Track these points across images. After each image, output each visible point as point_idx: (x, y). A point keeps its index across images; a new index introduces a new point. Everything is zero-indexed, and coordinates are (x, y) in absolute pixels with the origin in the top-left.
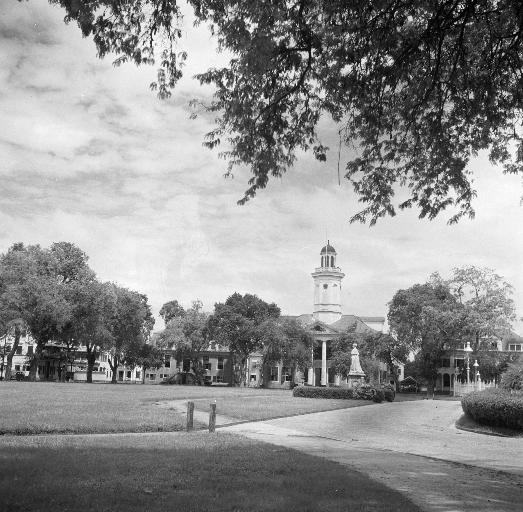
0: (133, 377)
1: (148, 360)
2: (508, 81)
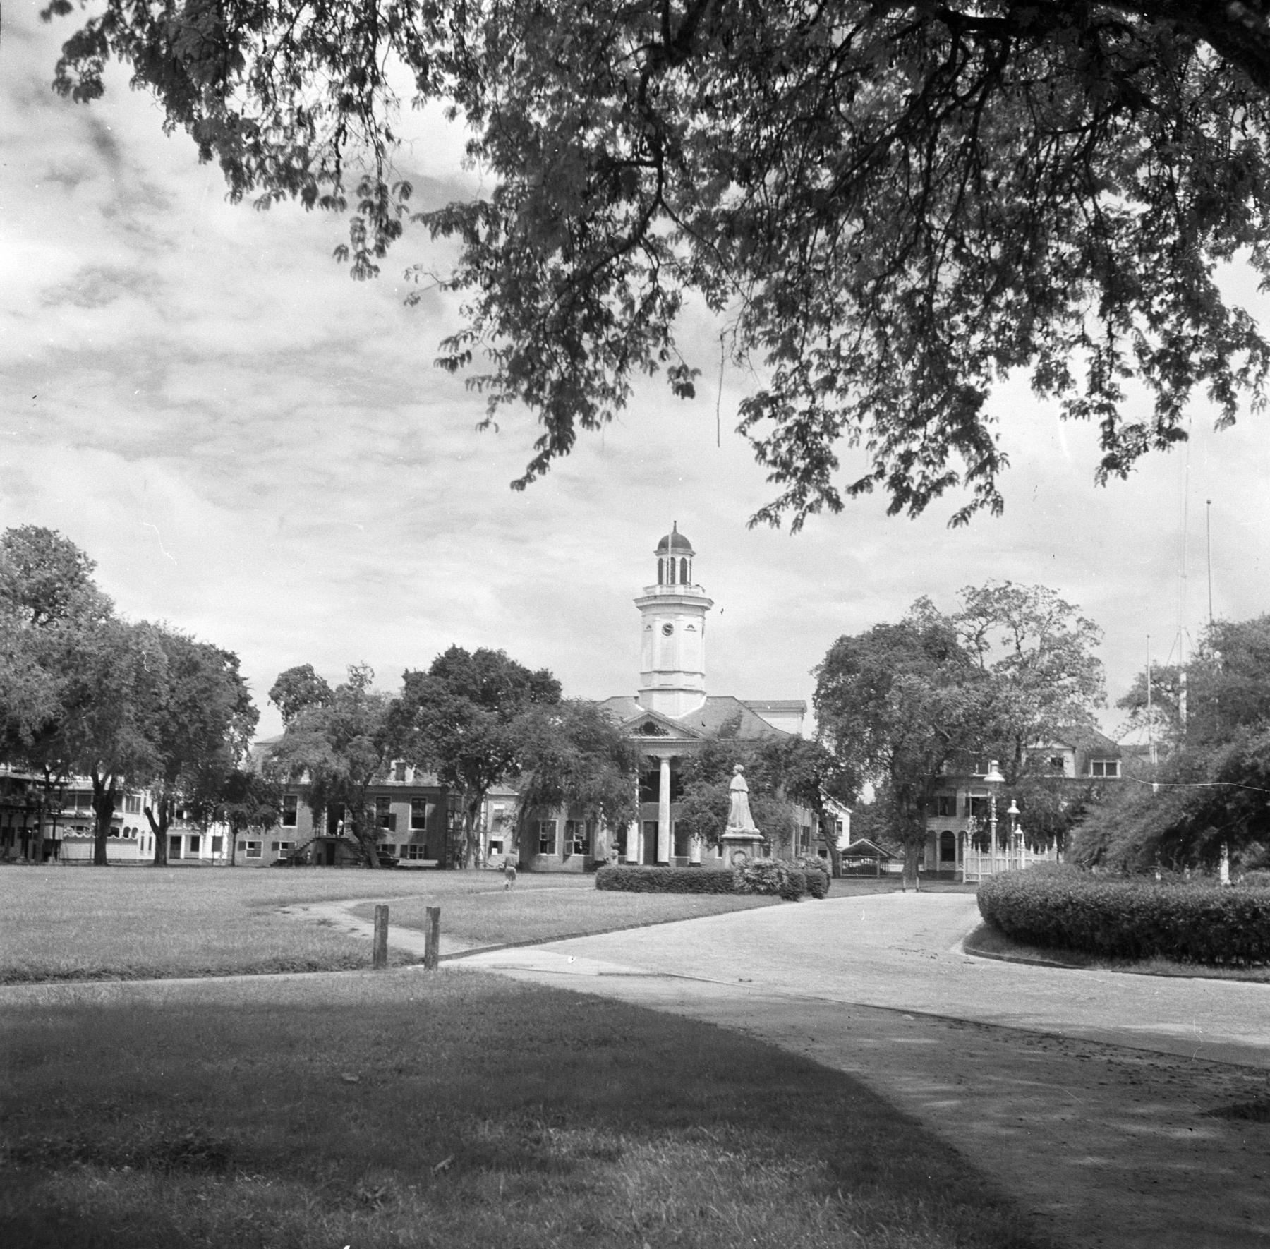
0: (205, 851)
1: (242, 808)
2: (1070, 223)
